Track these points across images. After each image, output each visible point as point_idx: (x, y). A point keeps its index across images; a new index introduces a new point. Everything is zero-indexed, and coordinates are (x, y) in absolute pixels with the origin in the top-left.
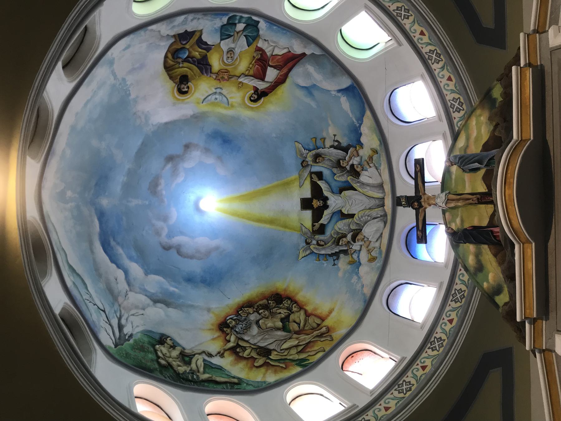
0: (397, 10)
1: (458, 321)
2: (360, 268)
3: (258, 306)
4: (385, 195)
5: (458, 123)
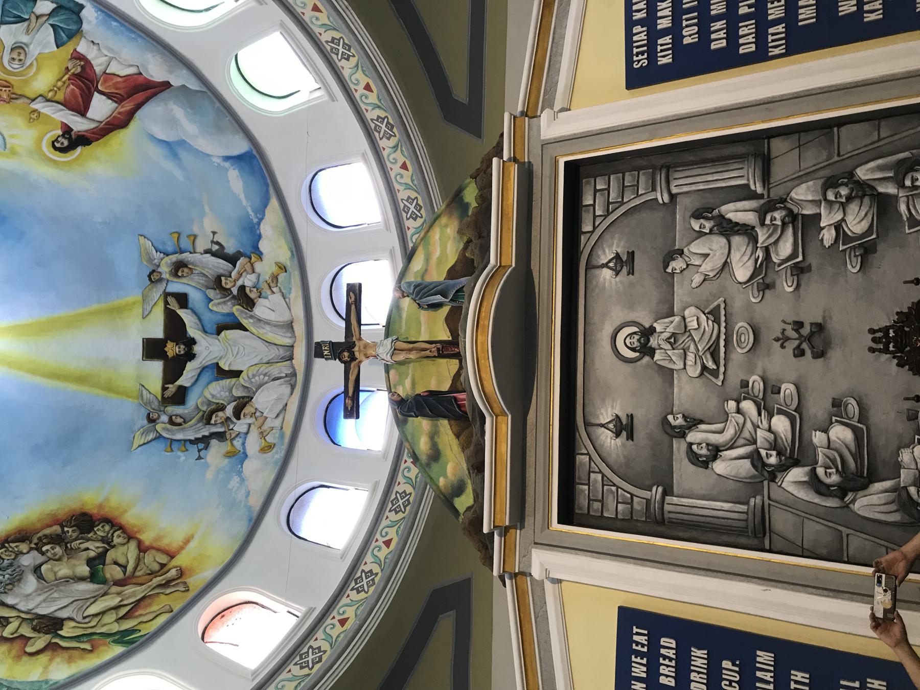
0: (332, 42)
1: (398, 543)
2: (247, 464)
3: (40, 539)
4: (295, 342)
5: (412, 236)
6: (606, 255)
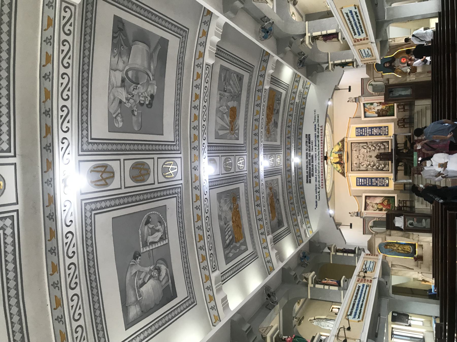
6: (354, 150)
